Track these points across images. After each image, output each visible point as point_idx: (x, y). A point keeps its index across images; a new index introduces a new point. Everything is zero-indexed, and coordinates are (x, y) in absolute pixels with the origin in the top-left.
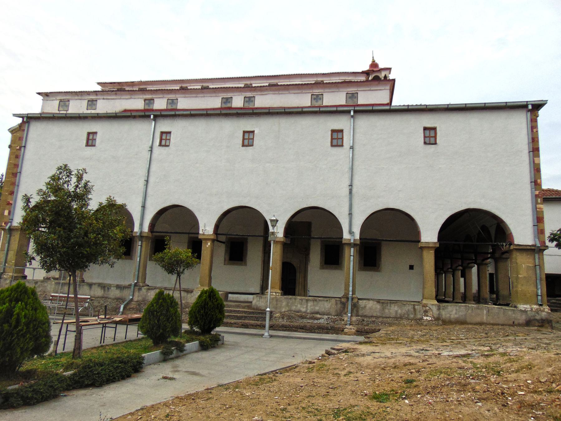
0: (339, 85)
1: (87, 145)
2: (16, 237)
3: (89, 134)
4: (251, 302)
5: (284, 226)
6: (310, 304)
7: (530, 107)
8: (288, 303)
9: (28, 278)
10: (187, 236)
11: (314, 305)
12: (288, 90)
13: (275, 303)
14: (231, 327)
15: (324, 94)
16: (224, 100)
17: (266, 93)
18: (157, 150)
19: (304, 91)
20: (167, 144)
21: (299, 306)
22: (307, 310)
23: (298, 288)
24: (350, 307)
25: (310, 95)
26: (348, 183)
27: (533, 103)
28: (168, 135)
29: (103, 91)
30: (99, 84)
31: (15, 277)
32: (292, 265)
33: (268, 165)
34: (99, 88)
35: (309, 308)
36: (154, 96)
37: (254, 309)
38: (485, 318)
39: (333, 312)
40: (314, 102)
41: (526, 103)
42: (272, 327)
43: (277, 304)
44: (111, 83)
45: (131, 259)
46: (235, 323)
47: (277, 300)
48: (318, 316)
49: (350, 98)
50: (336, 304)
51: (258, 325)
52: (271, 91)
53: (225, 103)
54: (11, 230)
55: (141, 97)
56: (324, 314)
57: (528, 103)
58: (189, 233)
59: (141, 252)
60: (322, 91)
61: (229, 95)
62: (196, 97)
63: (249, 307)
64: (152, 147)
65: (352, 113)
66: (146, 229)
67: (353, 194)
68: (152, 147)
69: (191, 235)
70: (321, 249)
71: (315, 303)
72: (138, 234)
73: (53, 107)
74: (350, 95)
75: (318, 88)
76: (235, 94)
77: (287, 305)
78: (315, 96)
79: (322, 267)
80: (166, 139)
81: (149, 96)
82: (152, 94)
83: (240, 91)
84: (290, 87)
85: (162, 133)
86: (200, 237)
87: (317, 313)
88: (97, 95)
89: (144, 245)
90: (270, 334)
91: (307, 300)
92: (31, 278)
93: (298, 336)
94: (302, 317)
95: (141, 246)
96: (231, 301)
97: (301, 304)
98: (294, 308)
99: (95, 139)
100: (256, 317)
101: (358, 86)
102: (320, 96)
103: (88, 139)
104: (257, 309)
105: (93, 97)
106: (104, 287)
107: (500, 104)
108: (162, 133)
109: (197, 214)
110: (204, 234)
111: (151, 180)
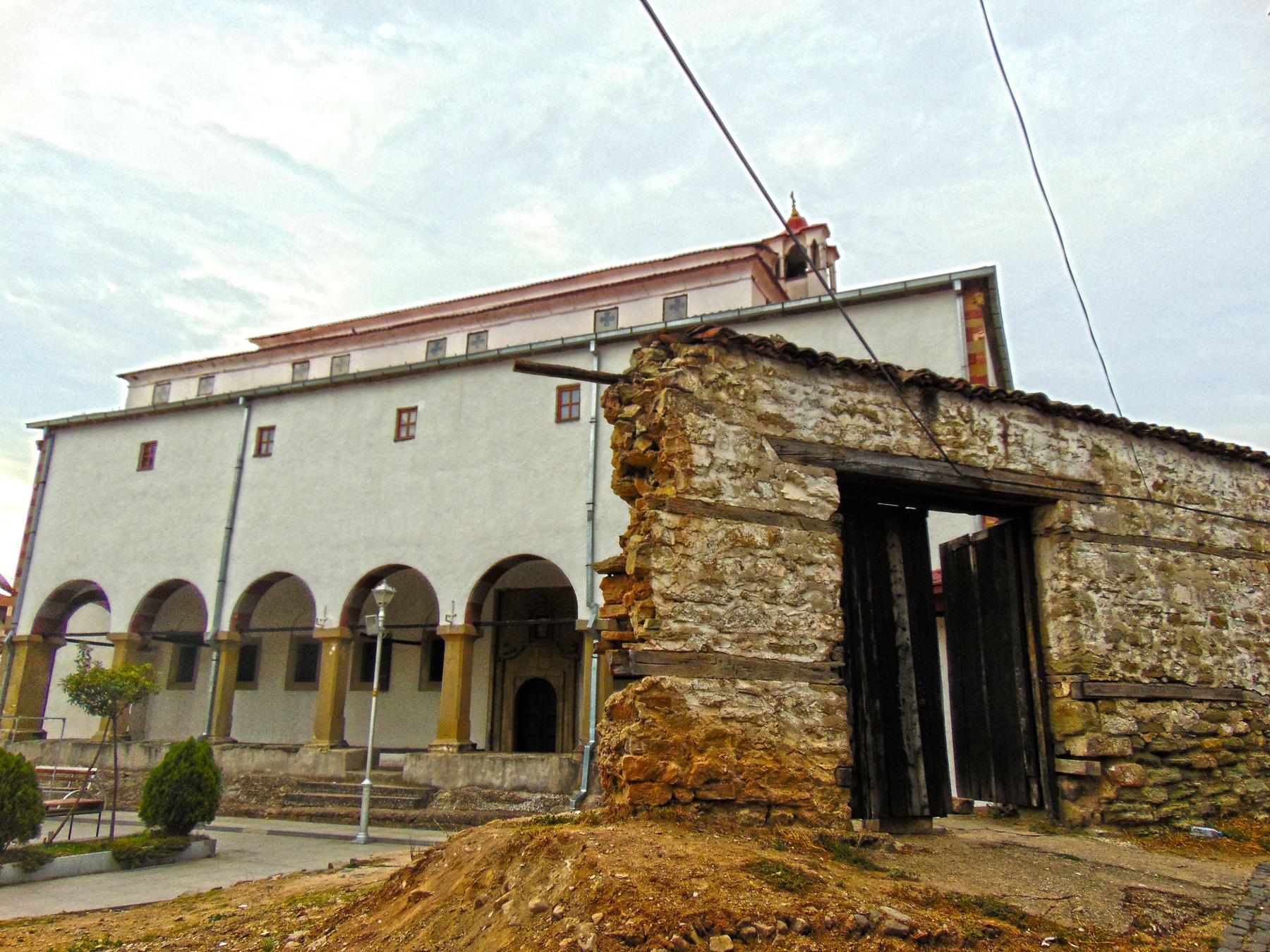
0: (647, 283)
1: (398, 438)
2: (22, 654)
3: (400, 412)
4: (401, 769)
5: (466, 601)
6: (510, 769)
7: (958, 286)
8: (468, 767)
9: (48, 737)
10: (288, 634)
11: (517, 771)
12: (548, 308)
13: (443, 766)
14: (339, 822)
15: (620, 307)
16: (432, 346)
17: (507, 320)
18: (251, 464)
19: (579, 307)
20: (575, 415)
21: (489, 773)
22: (503, 783)
23: (562, 735)
24: (585, 774)
25: (592, 312)
26: (589, 498)
27: (964, 276)
28: (575, 393)
29: (259, 351)
30: (254, 340)
31: (17, 735)
32: (549, 685)
33: (439, 474)
34: (254, 347)
35: (508, 778)
36: (309, 355)
37: (405, 783)
38: (691, 778)
39: (553, 786)
40: (601, 327)
41: (947, 279)
42: (374, 821)
43: (448, 771)
44: (273, 336)
45: (316, 689)
46: (347, 815)
47: (448, 763)
48: (524, 795)
49: (672, 307)
50: (561, 767)
51: (388, 819)
52: (516, 314)
53: (434, 351)
54: (13, 644)
55: (287, 358)
56: (535, 790)
57: (953, 277)
58: (292, 629)
59: (216, 673)
60: (616, 301)
61: (439, 334)
62: (382, 346)
63: (398, 780)
64: (241, 461)
65: (592, 348)
66: (226, 626)
67: (596, 522)
68: (241, 461)
69: (297, 633)
70: (290, 651)
71: (520, 766)
72: (590, 625)
73: (145, 397)
74: (672, 302)
75: (606, 296)
76: (623, 299)
77: (467, 773)
78: (602, 314)
79: (288, 687)
80: (571, 405)
81: (300, 356)
82: (304, 351)
83: (460, 324)
84: (551, 301)
85: (261, 430)
86: (316, 635)
87: (523, 788)
88: (214, 365)
89: (223, 659)
90: (371, 834)
91: (505, 761)
92: (57, 737)
93: (292, 829)
94: (491, 798)
95: (218, 660)
96: (384, 768)
97: (493, 769)
98: (478, 779)
99: (414, 424)
100: (393, 801)
101: (617, 294)
102: (612, 313)
103: (399, 425)
104: (411, 783)
105: (208, 371)
106: (150, 748)
107: (931, 281)
108: (261, 430)
109: (431, 579)
110: (322, 629)
111: (239, 525)
